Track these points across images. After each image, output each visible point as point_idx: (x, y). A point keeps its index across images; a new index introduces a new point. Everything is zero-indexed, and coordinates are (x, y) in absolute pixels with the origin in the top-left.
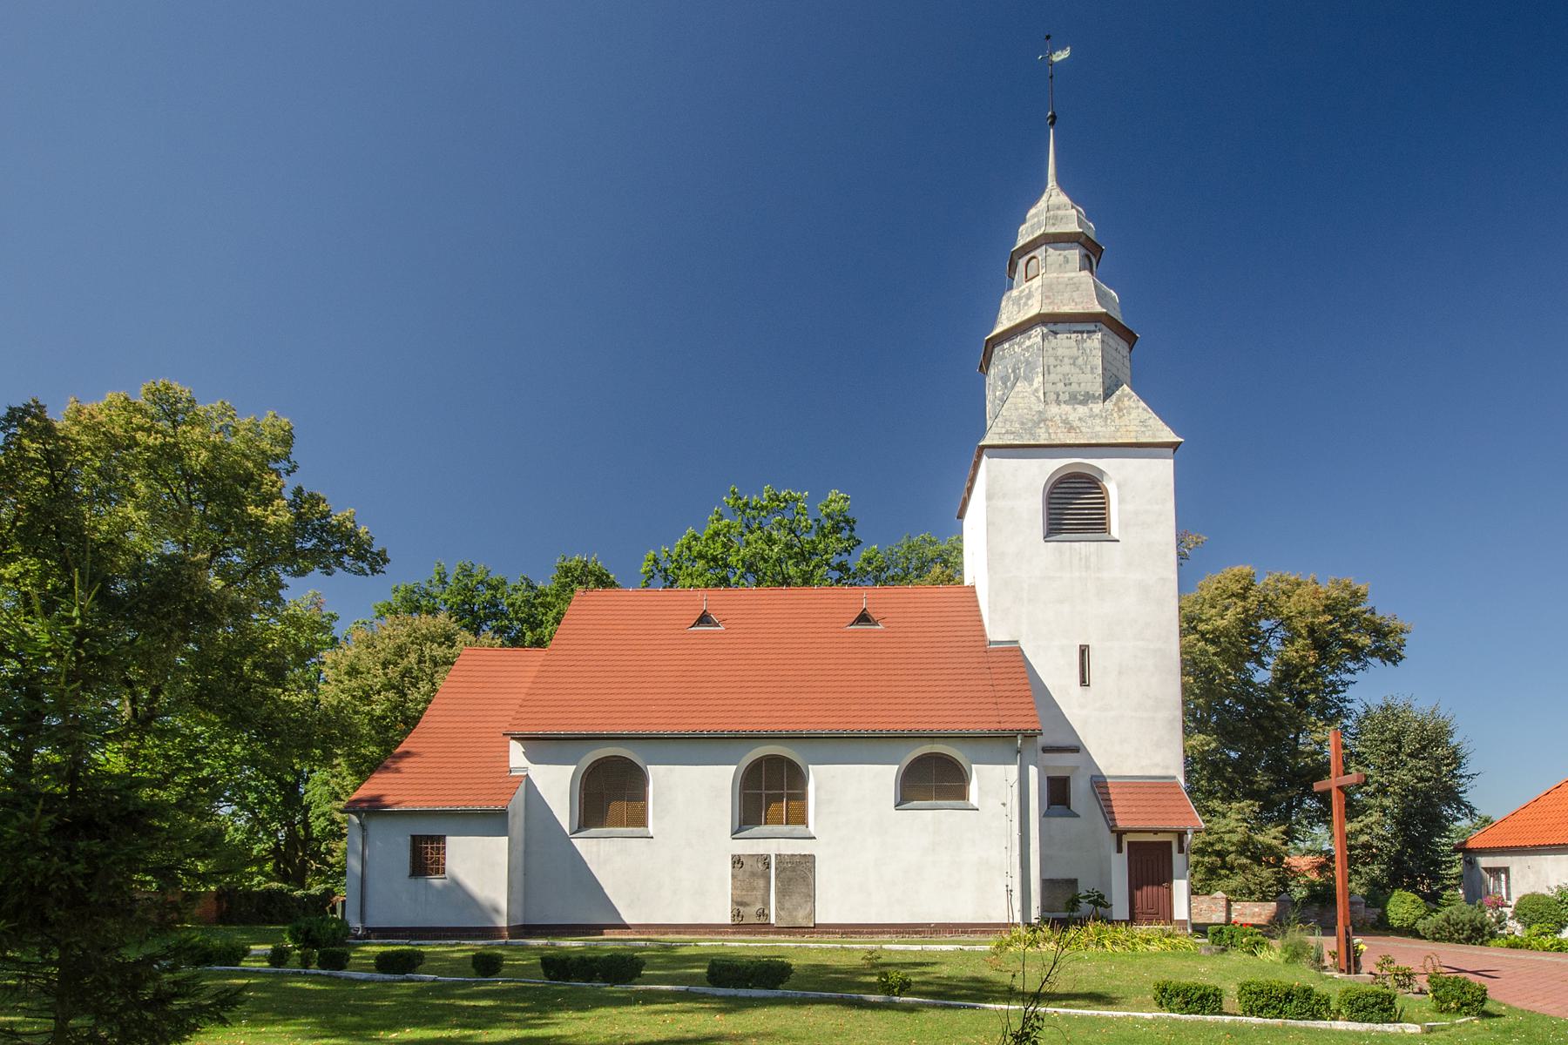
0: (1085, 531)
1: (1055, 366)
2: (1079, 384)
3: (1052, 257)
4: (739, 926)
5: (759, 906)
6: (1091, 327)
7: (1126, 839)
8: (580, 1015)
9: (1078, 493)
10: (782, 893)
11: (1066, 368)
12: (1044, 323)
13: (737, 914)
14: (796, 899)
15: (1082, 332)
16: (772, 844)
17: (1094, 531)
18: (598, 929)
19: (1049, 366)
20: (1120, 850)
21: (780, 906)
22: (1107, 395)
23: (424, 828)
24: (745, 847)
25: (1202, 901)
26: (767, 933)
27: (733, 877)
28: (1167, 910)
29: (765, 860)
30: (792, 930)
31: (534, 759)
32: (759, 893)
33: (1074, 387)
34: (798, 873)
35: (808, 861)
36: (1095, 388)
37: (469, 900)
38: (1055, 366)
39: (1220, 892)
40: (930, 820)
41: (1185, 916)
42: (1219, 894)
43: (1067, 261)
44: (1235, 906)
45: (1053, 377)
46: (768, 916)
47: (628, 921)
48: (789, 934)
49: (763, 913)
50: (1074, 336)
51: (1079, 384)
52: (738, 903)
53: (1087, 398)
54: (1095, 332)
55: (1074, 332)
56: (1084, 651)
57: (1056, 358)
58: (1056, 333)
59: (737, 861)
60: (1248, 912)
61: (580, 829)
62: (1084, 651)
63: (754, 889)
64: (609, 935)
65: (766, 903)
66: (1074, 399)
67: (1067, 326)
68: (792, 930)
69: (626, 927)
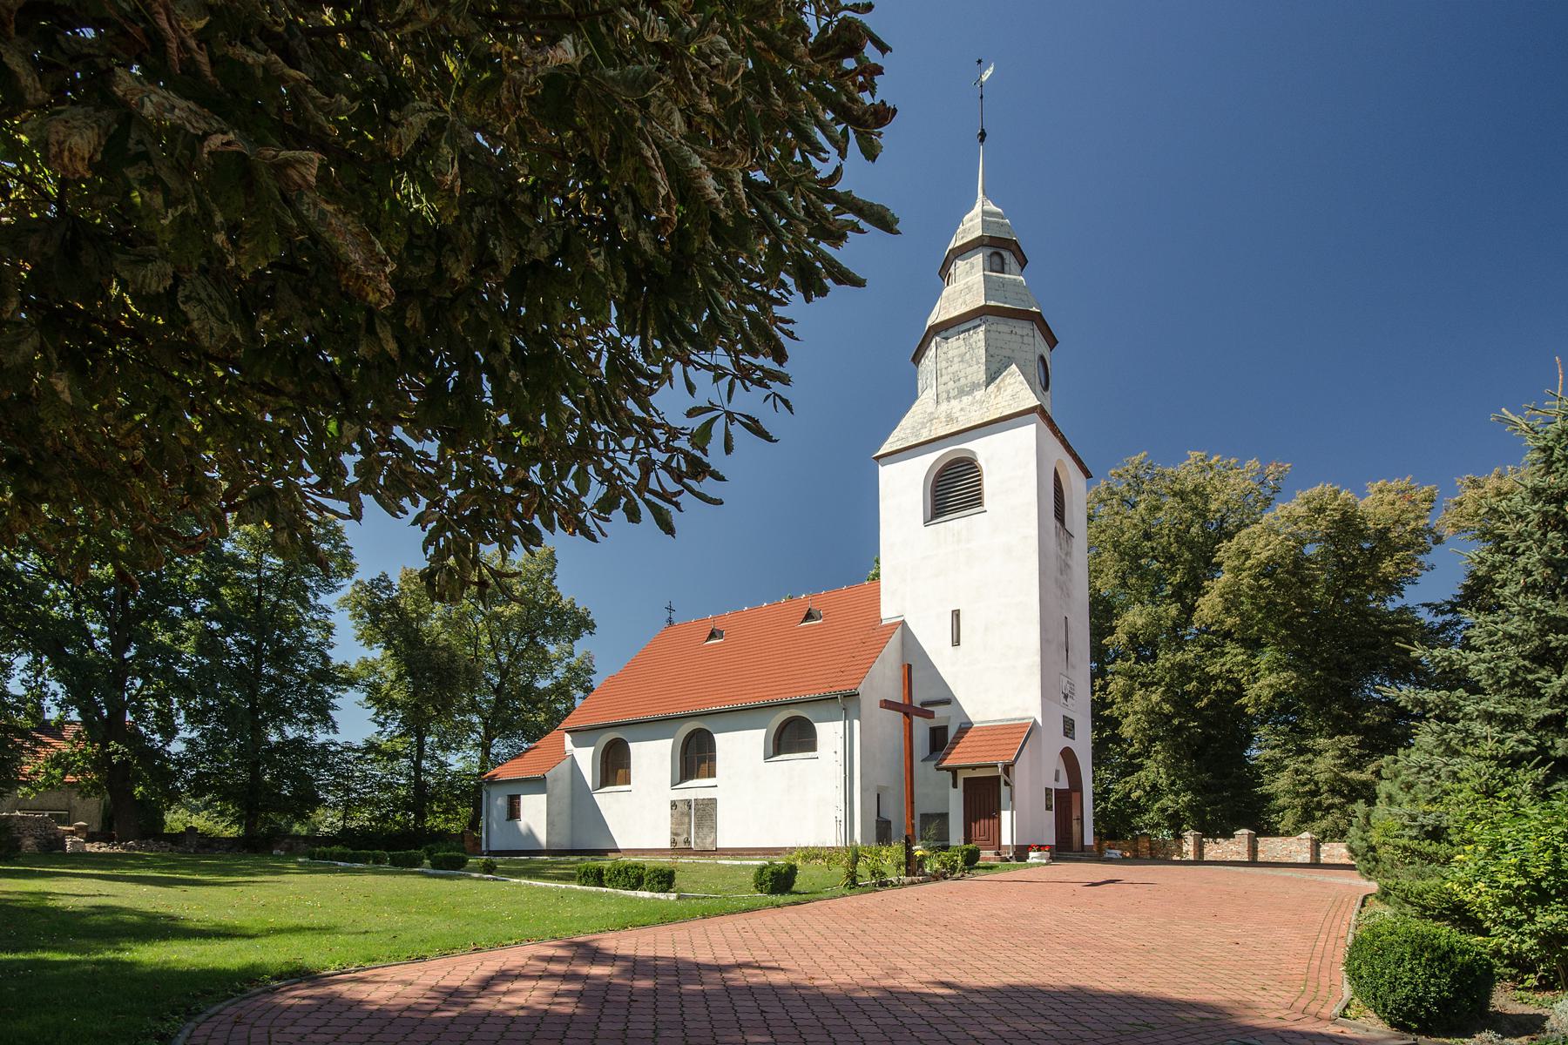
0: (965, 508)
1: (946, 368)
2: (966, 377)
3: (961, 268)
4: (675, 850)
5: (685, 836)
6: (977, 322)
7: (962, 776)
8: (275, 878)
9: (960, 476)
10: (698, 826)
11: (955, 367)
12: (937, 333)
13: (674, 842)
14: (706, 830)
15: (969, 330)
16: (696, 789)
17: (971, 507)
18: (603, 853)
19: (941, 370)
20: (955, 785)
21: (697, 836)
22: (991, 379)
23: (513, 791)
24: (680, 794)
25: (1291, 843)
26: (689, 855)
27: (672, 816)
28: (996, 837)
29: (688, 802)
30: (703, 852)
31: (576, 744)
32: (685, 827)
33: (963, 381)
34: (705, 812)
35: (713, 802)
36: (979, 377)
37: (531, 834)
38: (946, 368)
39: (1307, 833)
40: (793, 764)
41: (1009, 843)
42: (1306, 835)
43: (972, 267)
44: (1324, 848)
45: (945, 378)
46: (690, 843)
47: (620, 847)
48: (701, 855)
49: (687, 841)
50: (961, 336)
51: (966, 377)
52: (675, 834)
53: (974, 387)
54: (980, 325)
55: (963, 332)
56: (956, 614)
57: (947, 360)
58: (947, 338)
59: (674, 805)
60: (1336, 853)
61: (603, 785)
62: (956, 614)
63: (682, 824)
64: (612, 856)
65: (689, 834)
66: (962, 392)
67: (956, 329)
68: (703, 852)
69: (618, 851)
